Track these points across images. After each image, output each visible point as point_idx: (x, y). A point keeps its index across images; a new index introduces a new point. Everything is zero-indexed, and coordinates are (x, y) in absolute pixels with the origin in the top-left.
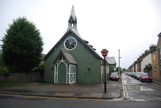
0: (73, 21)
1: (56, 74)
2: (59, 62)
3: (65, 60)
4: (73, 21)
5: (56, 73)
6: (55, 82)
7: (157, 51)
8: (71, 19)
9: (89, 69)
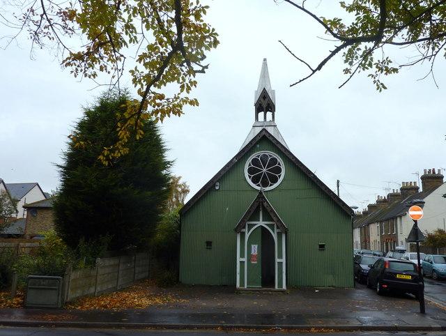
0: (265, 104)
1: (280, 264)
2: (250, 226)
3: (272, 220)
4: (265, 104)
5: (242, 260)
6: (238, 285)
7: (266, 128)
8: (262, 100)
9: (322, 247)
